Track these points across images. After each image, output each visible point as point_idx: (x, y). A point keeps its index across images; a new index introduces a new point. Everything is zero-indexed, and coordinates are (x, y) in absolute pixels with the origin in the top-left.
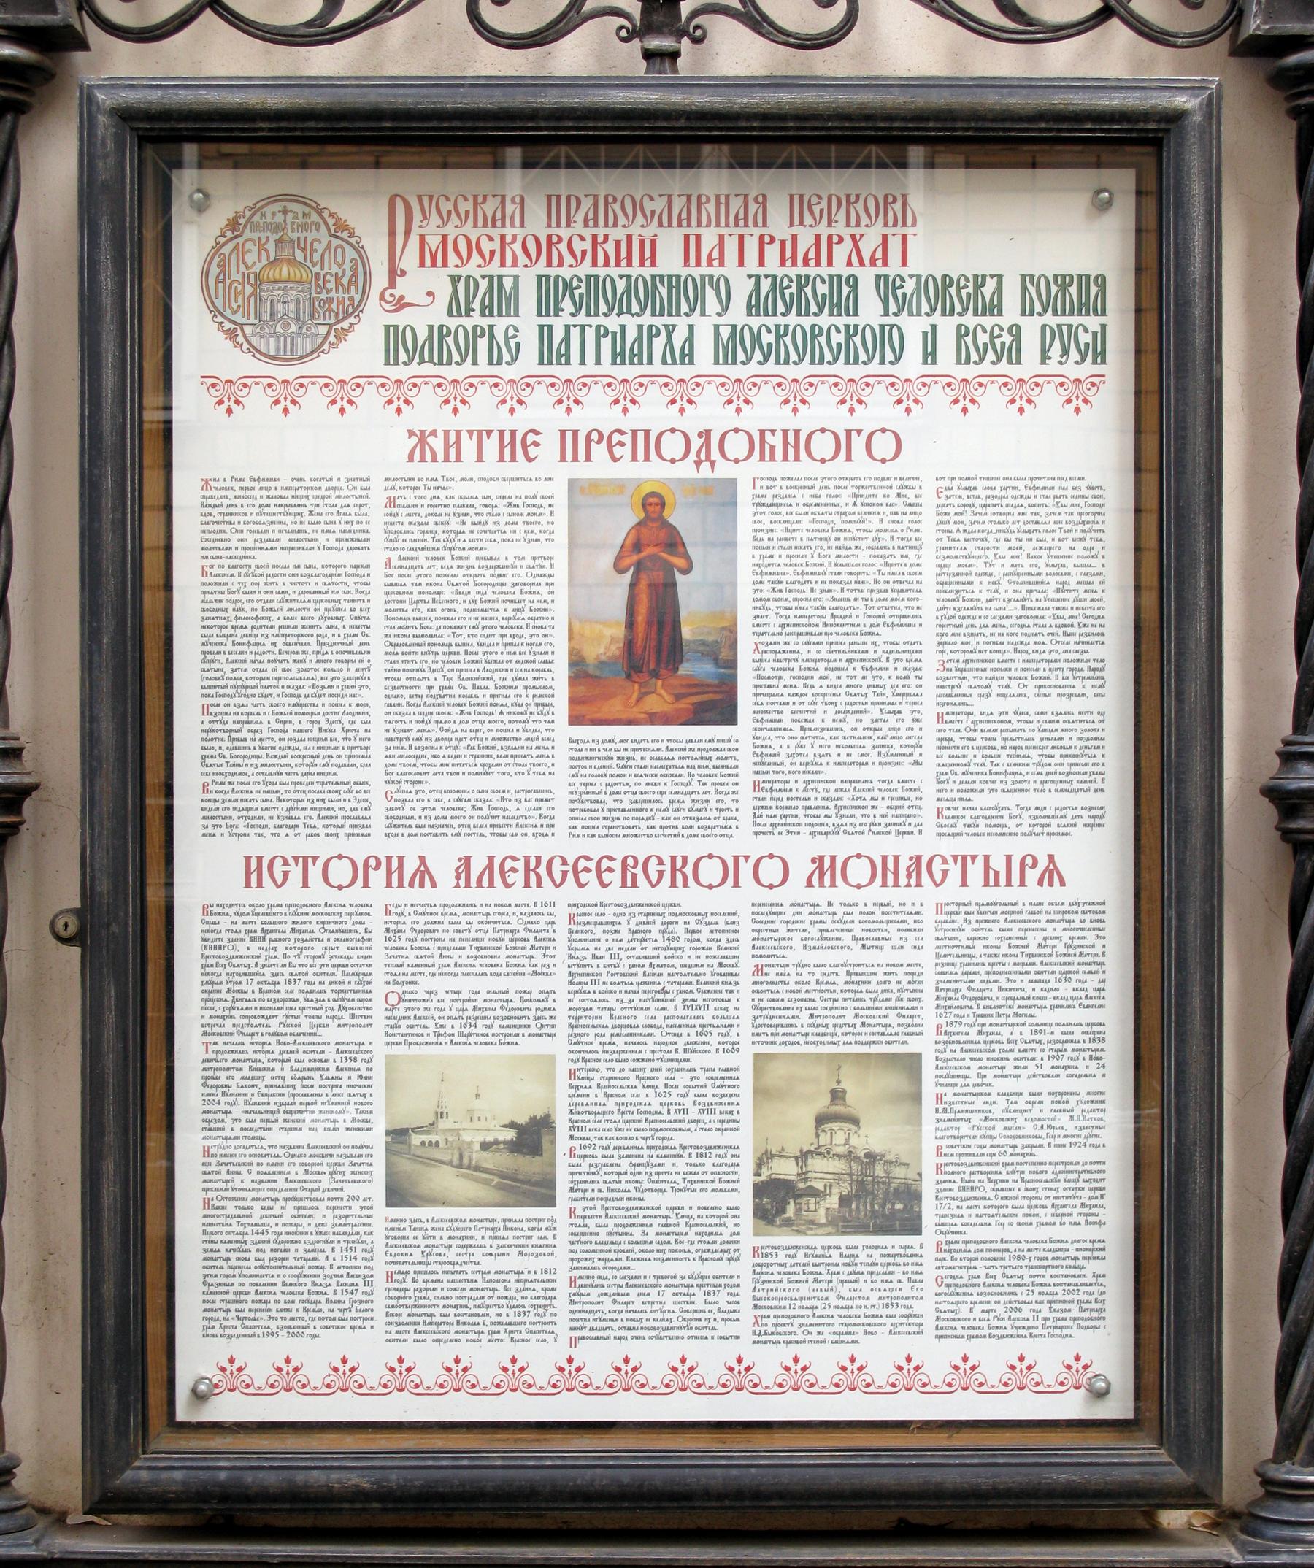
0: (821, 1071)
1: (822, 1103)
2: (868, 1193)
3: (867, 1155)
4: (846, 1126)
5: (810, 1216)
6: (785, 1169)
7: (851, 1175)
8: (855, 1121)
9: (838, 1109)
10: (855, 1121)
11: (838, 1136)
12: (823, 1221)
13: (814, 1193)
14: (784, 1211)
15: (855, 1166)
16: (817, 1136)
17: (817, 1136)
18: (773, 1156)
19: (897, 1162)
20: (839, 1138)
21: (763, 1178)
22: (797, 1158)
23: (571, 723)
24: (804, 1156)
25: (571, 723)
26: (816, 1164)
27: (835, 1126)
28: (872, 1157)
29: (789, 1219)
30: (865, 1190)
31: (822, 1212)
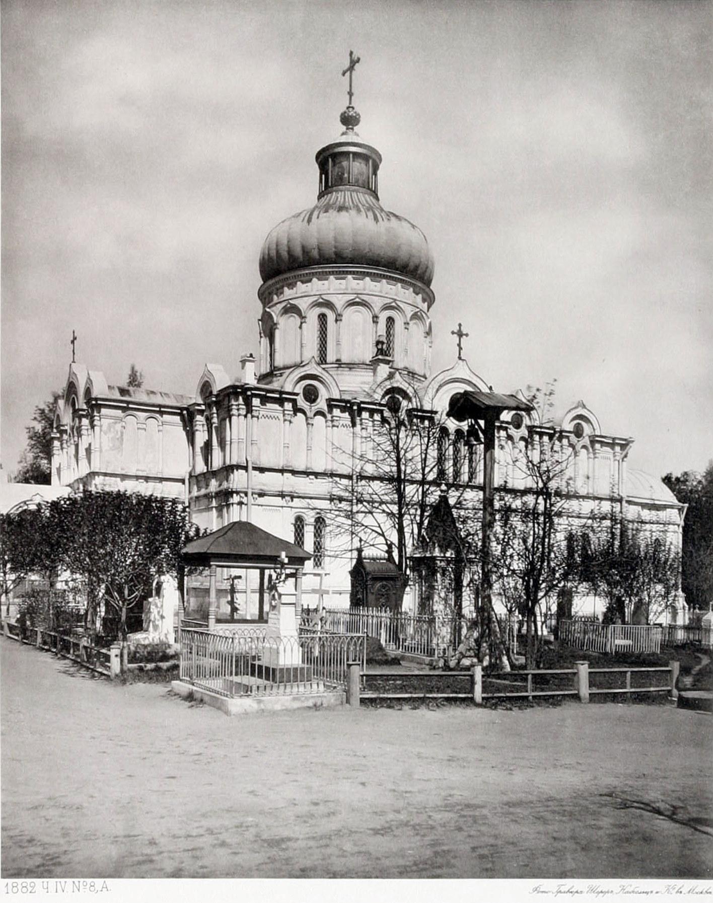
3: (462, 406)
4: (381, 290)
7: (397, 481)
9: (348, 225)
10: (413, 273)
11: (354, 316)
13: (250, 548)
15: (414, 446)
16: (269, 329)
17: (269, 329)
18: (94, 405)
19: (579, 433)
20: (355, 336)
21: (56, 491)
22: (187, 416)
23: (50, 484)
24: (221, 403)
25: (50, 484)
26: (260, 436)
27: (335, 287)
28: (478, 413)
30: (459, 544)
31: (287, 622)
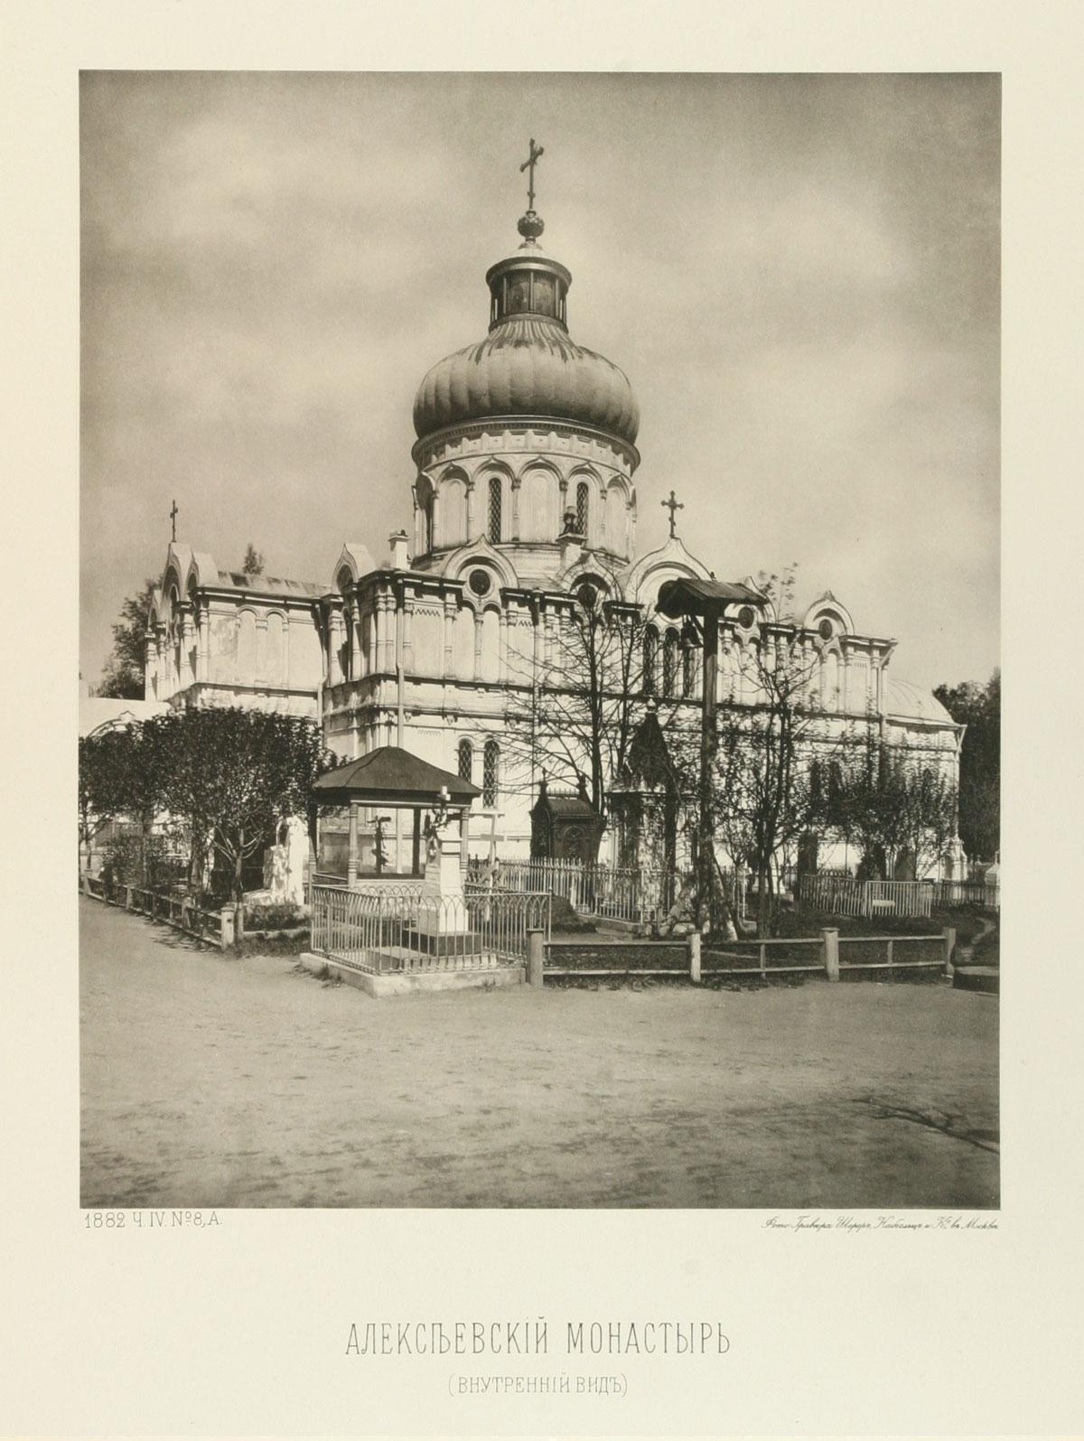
0: (419, 176)
1: (450, 336)
2: (676, 788)
3: (677, 597)
4: (569, 448)
5: (390, 898)
6: (264, 664)
7: (591, 695)
8: (613, 426)
9: (528, 363)
12: (454, 922)
13: (401, 780)
14: (256, 877)
15: (612, 649)
16: (425, 498)
17: (425, 498)
20: (537, 508)
21: (365, 703)
22: (321, 612)
23: (996, 77)
24: (362, 595)
25: (996, 77)
26: (416, 637)
27: (511, 445)
28: (697, 607)
29: (282, 918)
31: (449, 877)
